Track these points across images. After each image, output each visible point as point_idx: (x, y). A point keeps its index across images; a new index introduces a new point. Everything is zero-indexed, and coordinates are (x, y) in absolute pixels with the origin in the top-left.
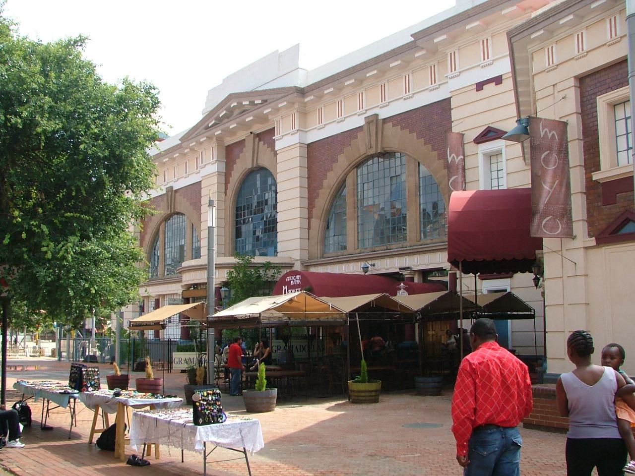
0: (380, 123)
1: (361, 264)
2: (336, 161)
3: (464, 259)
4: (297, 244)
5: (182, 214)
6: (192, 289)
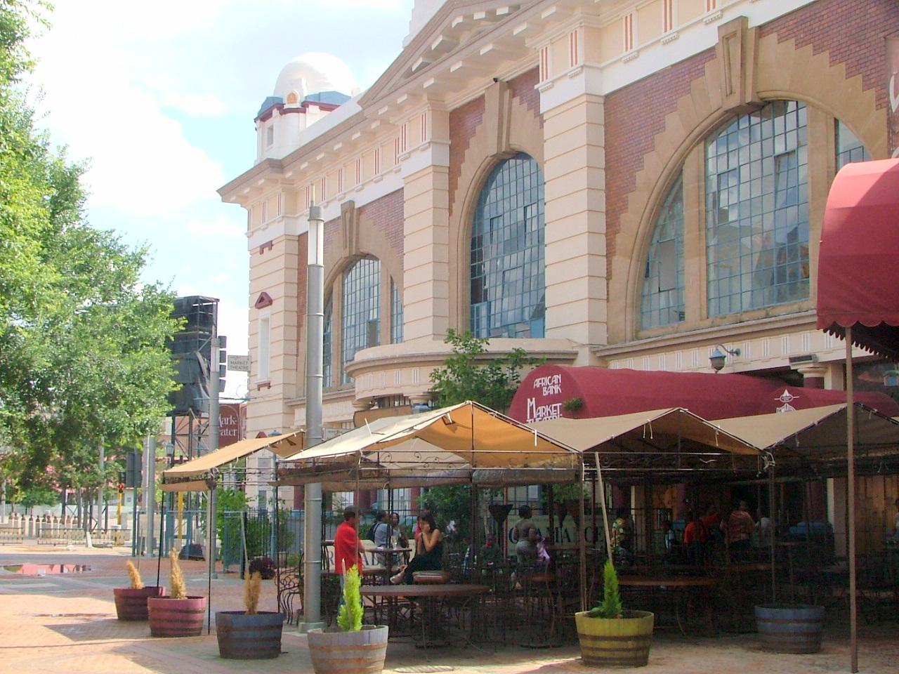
0: (751, 37)
1: (710, 351)
2: (662, 128)
3: (858, 322)
4: (581, 312)
5: (375, 258)
6: (376, 407)
